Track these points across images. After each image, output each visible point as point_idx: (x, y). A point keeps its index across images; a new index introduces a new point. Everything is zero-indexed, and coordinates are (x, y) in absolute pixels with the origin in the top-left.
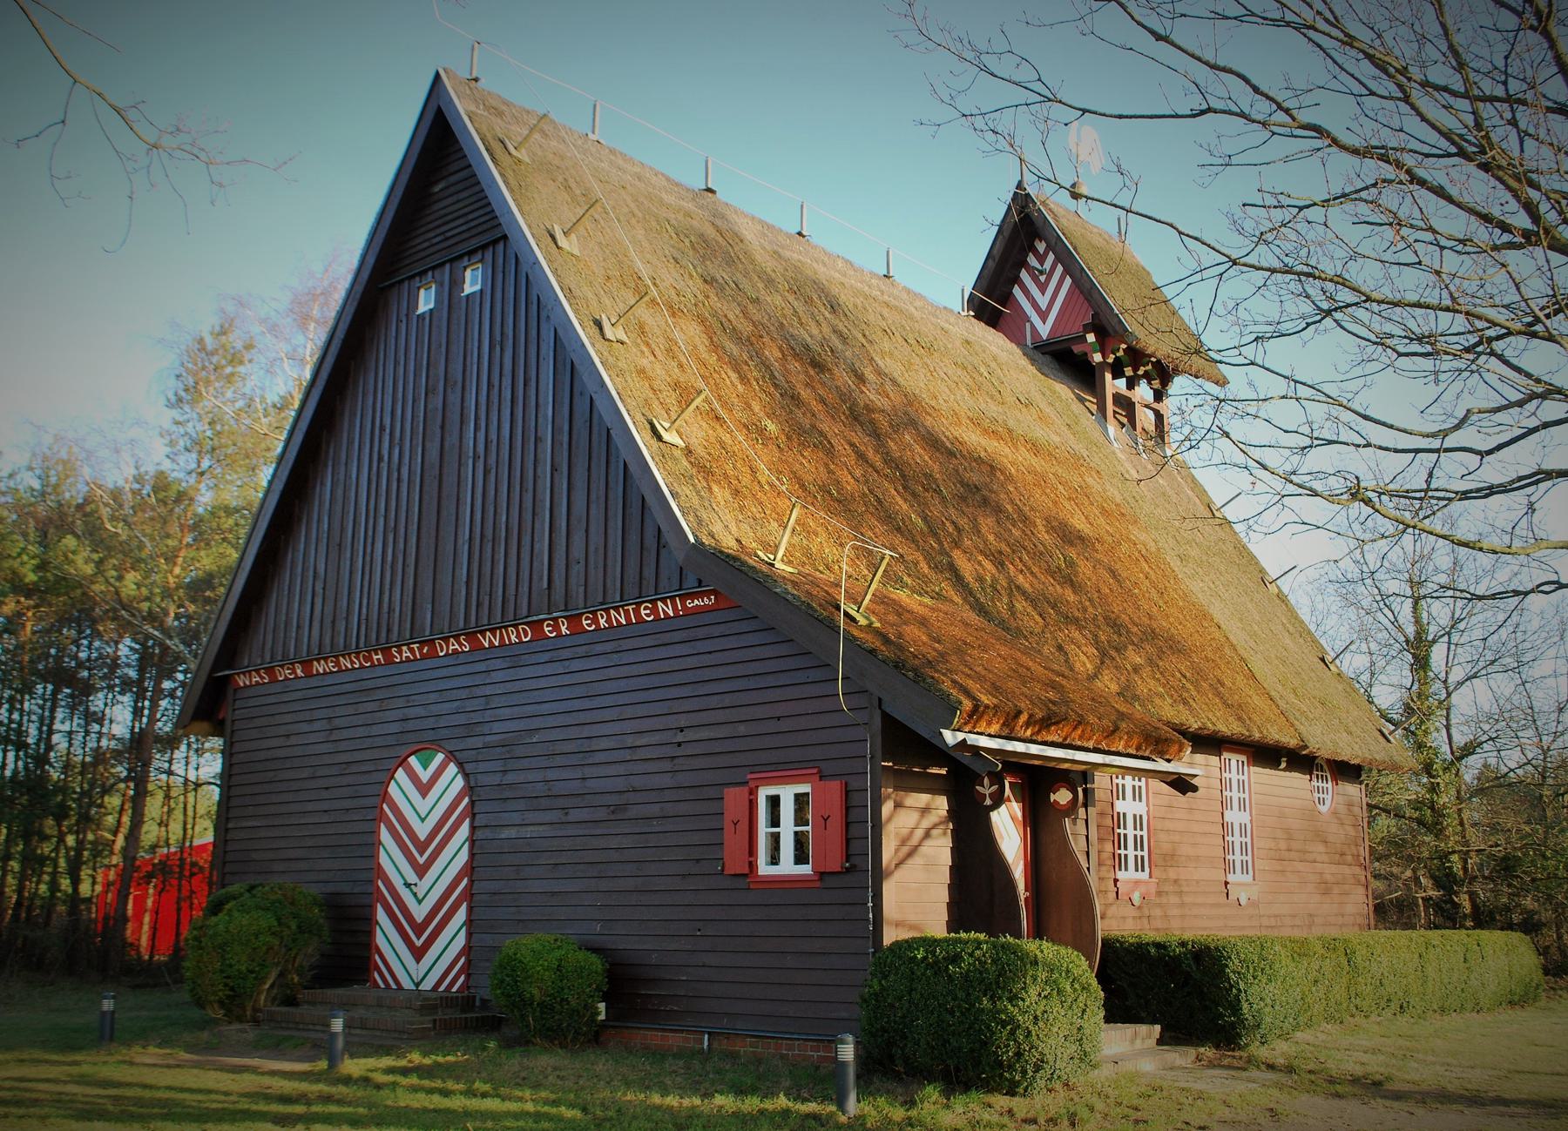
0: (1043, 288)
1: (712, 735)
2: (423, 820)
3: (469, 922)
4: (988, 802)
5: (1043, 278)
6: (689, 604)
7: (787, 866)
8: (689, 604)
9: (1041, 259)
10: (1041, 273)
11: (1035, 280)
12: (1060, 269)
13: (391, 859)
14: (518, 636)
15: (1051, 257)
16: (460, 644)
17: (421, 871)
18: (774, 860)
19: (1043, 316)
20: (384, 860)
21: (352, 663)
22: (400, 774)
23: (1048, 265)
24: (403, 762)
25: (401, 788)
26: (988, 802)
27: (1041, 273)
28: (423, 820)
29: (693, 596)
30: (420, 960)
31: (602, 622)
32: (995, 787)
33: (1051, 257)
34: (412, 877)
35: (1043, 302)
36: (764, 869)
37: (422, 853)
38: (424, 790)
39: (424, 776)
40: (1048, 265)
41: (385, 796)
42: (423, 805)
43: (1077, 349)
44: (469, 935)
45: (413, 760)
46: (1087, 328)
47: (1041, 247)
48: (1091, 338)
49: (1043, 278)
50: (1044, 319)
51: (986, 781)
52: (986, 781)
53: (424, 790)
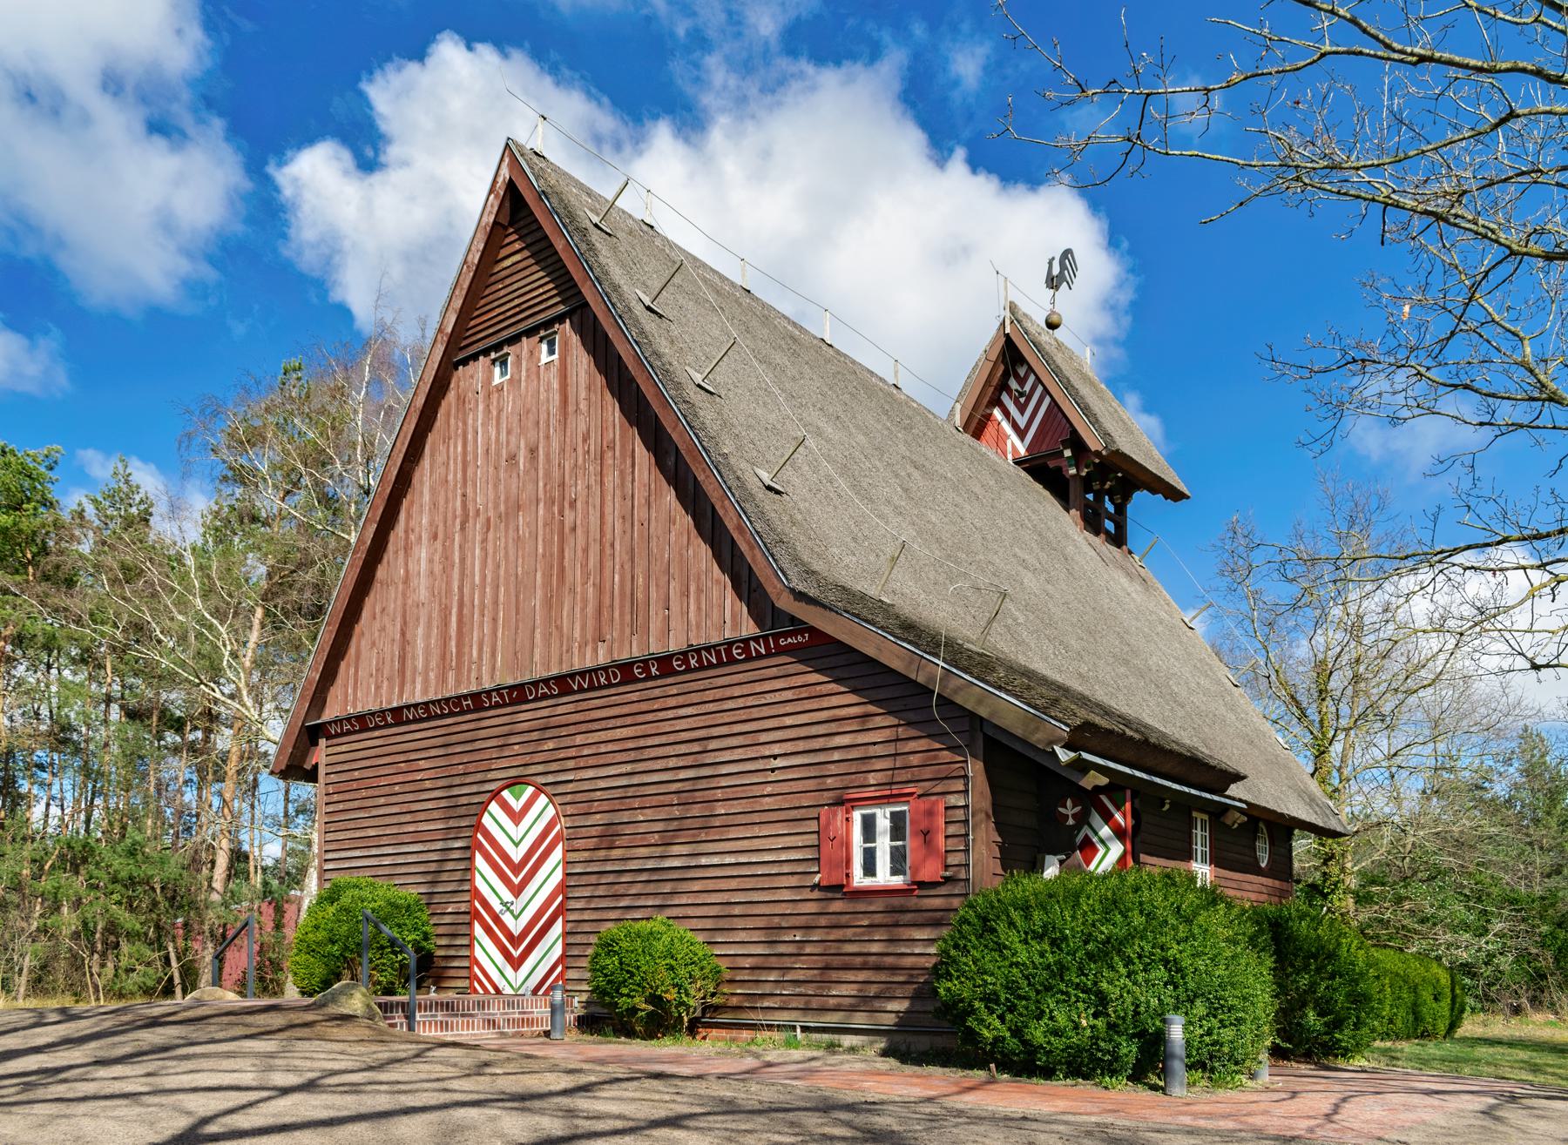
0: (1022, 409)
1: (807, 761)
2: (517, 845)
3: (566, 934)
4: (1071, 822)
5: (1022, 400)
6: (782, 642)
7: (884, 877)
8: (782, 642)
9: (1022, 382)
10: (1021, 394)
11: (1017, 403)
12: (1040, 389)
13: (486, 880)
14: (608, 678)
15: (1032, 379)
16: (550, 688)
17: (517, 891)
18: (870, 869)
19: (1021, 434)
20: (479, 883)
21: (442, 709)
22: (494, 807)
23: (1027, 388)
24: (495, 795)
25: (494, 819)
26: (1071, 822)
27: (1021, 394)
28: (517, 845)
29: (786, 635)
30: (1128, 793)
31: (693, 662)
32: (1078, 809)
33: (1032, 379)
34: (507, 896)
35: (1022, 422)
36: (859, 879)
37: (517, 875)
38: (516, 817)
39: (517, 805)
40: (1027, 388)
41: (479, 827)
42: (516, 832)
43: (1051, 464)
44: (566, 945)
45: (506, 794)
46: (1066, 444)
47: (1022, 372)
48: (1068, 453)
49: (1022, 400)
50: (1022, 438)
51: (1069, 803)
52: (1069, 803)
53: (516, 817)
